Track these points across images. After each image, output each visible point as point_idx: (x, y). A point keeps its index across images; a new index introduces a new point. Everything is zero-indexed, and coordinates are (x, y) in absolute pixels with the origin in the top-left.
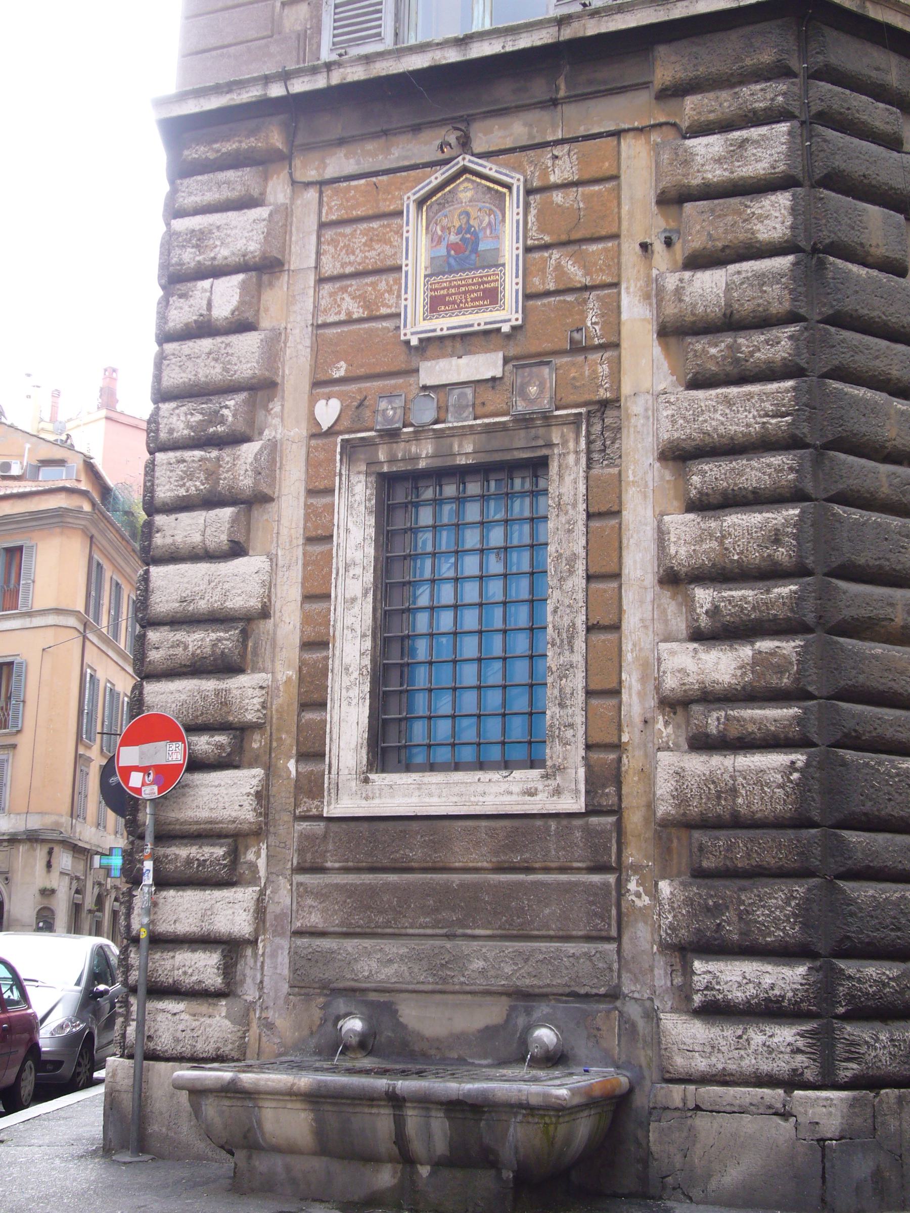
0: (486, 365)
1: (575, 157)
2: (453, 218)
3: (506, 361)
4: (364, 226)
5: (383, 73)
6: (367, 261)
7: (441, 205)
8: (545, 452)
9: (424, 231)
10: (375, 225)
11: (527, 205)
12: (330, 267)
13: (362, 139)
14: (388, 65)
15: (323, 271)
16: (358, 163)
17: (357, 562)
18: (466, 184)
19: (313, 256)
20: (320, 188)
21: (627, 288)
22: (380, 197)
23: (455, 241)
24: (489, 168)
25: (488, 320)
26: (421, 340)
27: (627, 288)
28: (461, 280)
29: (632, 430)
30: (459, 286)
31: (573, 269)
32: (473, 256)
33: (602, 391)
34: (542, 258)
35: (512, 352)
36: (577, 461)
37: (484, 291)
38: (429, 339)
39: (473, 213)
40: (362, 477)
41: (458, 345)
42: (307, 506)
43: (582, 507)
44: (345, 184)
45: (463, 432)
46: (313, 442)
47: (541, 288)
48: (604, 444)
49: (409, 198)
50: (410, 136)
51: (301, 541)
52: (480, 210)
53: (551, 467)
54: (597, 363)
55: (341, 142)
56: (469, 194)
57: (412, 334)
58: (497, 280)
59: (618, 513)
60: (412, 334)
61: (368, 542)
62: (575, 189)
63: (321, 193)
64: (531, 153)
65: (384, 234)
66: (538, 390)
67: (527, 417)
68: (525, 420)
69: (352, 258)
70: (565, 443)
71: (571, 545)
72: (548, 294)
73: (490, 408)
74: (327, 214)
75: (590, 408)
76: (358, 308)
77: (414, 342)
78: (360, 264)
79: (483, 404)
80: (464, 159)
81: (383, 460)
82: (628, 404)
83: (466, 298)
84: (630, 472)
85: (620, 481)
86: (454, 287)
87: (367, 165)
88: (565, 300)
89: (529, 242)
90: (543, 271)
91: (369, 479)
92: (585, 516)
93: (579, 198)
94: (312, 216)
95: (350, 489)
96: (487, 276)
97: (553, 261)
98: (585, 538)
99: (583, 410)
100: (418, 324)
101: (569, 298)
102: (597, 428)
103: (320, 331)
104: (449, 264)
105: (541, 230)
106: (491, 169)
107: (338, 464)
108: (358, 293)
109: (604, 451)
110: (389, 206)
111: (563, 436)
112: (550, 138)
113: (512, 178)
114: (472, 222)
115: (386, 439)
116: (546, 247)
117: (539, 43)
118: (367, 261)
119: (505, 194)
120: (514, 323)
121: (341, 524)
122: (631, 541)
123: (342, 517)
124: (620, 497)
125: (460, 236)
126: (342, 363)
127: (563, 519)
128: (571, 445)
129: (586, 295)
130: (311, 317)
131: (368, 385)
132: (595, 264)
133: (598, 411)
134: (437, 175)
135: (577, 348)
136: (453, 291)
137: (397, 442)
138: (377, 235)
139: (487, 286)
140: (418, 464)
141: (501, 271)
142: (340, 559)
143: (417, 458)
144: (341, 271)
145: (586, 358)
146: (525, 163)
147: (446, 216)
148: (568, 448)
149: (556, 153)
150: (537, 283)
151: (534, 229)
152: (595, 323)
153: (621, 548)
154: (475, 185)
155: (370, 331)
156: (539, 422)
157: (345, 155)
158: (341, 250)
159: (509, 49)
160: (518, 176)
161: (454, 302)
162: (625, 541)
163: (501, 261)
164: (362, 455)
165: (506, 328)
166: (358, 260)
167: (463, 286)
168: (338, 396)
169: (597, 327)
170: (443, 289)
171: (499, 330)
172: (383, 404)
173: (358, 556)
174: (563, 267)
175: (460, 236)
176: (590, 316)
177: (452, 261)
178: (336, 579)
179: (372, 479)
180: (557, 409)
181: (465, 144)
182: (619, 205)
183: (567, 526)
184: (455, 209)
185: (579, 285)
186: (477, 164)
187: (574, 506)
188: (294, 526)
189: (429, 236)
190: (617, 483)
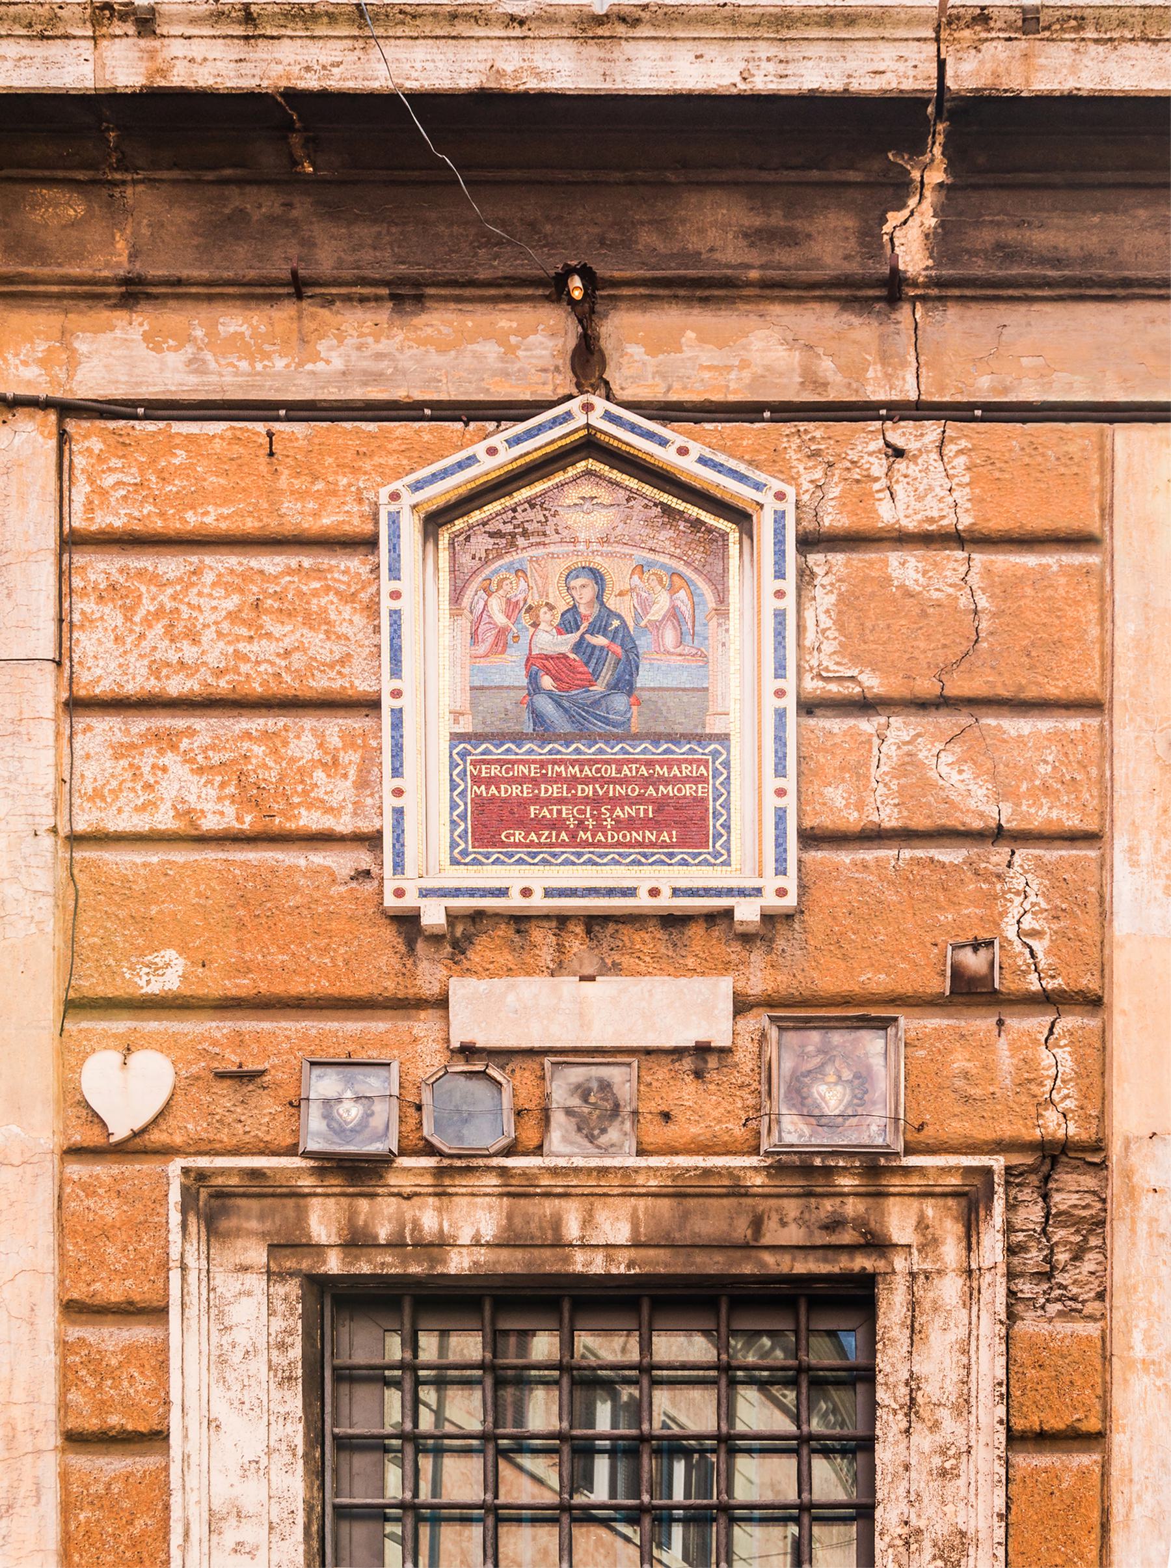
0: (685, 1006)
1: (962, 460)
2: (543, 576)
3: (742, 1006)
4: (232, 561)
5: (311, 83)
6: (245, 668)
7: (507, 540)
8: (862, 1263)
9: (445, 604)
10: (270, 563)
11: (805, 576)
12: (104, 667)
13: (210, 298)
14: (325, 59)
15: (84, 677)
16: (196, 365)
17: (249, 1507)
18: (588, 488)
19: (51, 628)
20: (60, 421)
21: (1132, 850)
22: (283, 482)
23: (551, 650)
24: (681, 451)
25: (683, 884)
26: (452, 917)
27: (1132, 850)
28: (581, 763)
29: (1142, 1228)
30: (573, 781)
31: (955, 777)
32: (619, 701)
33: (1052, 1118)
34: (853, 733)
35: (758, 983)
36: (971, 1296)
37: (661, 804)
38: (477, 916)
39: (618, 575)
40: (256, 1282)
41: (576, 944)
42: (64, 1347)
43: (989, 1413)
44: (151, 426)
45: (598, 1186)
46: (77, 1170)
47: (852, 820)
48: (1048, 1260)
49: (395, 496)
50: (383, 314)
51: (51, 1439)
52: (640, 569)
53: (882, 1306)
54: (1036, 1041)
55: (132, 292)
56: (601, 519)
57: (425, 893)
58: (702, 779)
59: (1096, 1439)
60: (425, 893)
61: (279, 1461)
62: (960, 555)
63: (63, 438)
64: (816, 430)
65: (301, 594)
66: (848, 1092)
67: (818, 1162)
68: (807, 1170)
69: (189, 652)
70: (929, 1243)
71: (950, 1509)
72: (873, 836)
73: (686, 1129)
74: (89, 507)
75: (1016, 1159)
76: (220, 799)
77: (433, 916)
78: (219, 673)
79: (666, 1116)
80: (588, 408)
81: (324, 1240)
82: (1134, 1159)
83: (598, 818)
84: (1137, 1336)
85: (1106, 1358)
86: (558, 779)
87: (228, 379)
88: (932, 860)
89: (812, 686)
90: (858, 772)
91: (280, 1290)
92: (1002, 1437)
93: (974, 579)
94: (34, 504)
95: (215, 1310)
96: (669, 764)
97: (889, 748)
98: (1001, 1491)
99: (998, 1163)
100: (431, 869)
101: (951, 855)
102: (1032, 1214)
103: (84, 854)
104: (538, 717)
105: (849, 652)
106: (683, 451)
107: (175, 1235)
108: (215, 758)
109: (1048, 1276)
110: (316, 515)
111: (922, 1225)
112: (877, 393)
113: (758, 487)
114: (612, 603)
115: (335, 1183)
116: (865, 705)
117: (867, 85)
118: (245, 668)
119: (724, 536)
120: (770, 901)
121: (192, 1402)
122: (1138, 1511)
123: (192, 1384)
124: (1105, 1398)
125: (574, 637)
126: (170, 954)
127: (923, 1440)
128: (951, 1251)
129: (998, 855)
130: (48, 808)
131: (266, 1025)
132: (1028, 773)
133: (1033, 1170)
134: (497, 441)
135: (970, 992)
136: (554, 791)
137: (372, 1196)
138: (279, 596)
139: (670, 790)
140: (444, 1262)
141: (716, 754)
142: (193, 1497)
143: (442, 1244)
144: (152, 686)
145: (1000, 1023)
146: (792, 455)
147: (520, 572)
148: (939, 1258)
149: (900, 442)
150: (840, 803)
151: (828, 647)
152: (1034, 933)
153: (1105, 1527)
154: (622, 494)
155: (269, 879)
156: (846, 1182)
157: (146, 337)
158: (148, 622)
159: (764, 82)
160: (777, 485)
161: (556, 825)
162: (1118, 1511)
163: (715, 726)
164: (250, 1217)
165: (747, 912)
166: (213, 659)
167: (586, 781)
168: (165, 1045)
169: (1038, 946)
170: (521, 780)
171: (728, 913)
172: (324, 1085)
173: (252, 1494)
174: (920, 765)
175: (574, 637)
176: (1015, 911)
177: (547, 706)
178: (184, 1548)
179: (292, 1288)
180: (909, 1150)
181: (588, 363)
182: (1106, 618)
183: (937, 1461)
184: (552, 556)
185: (977, 824)
186: (633, 428)
187: (964, 1405)
188: (19, 1395)
189: (465, 623)
190: (1098, 1362)
